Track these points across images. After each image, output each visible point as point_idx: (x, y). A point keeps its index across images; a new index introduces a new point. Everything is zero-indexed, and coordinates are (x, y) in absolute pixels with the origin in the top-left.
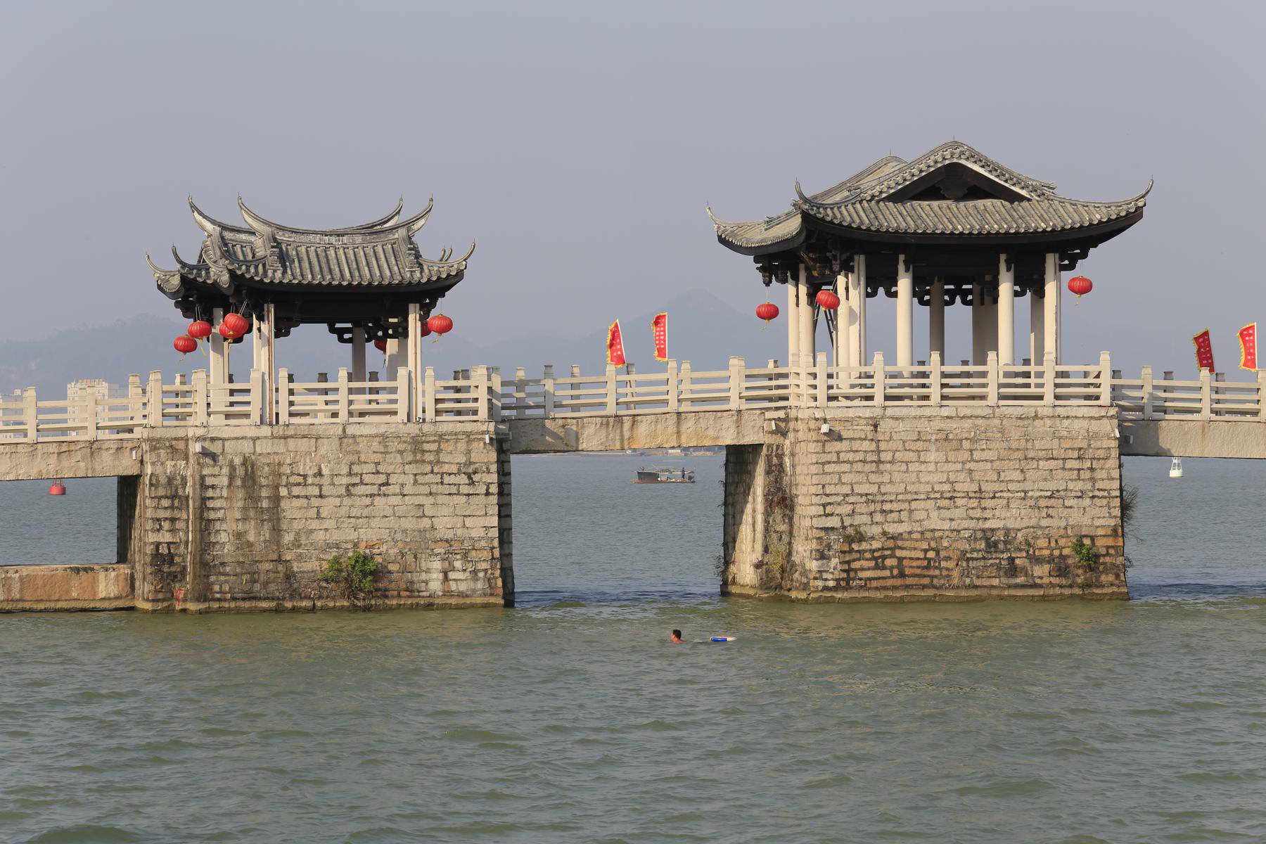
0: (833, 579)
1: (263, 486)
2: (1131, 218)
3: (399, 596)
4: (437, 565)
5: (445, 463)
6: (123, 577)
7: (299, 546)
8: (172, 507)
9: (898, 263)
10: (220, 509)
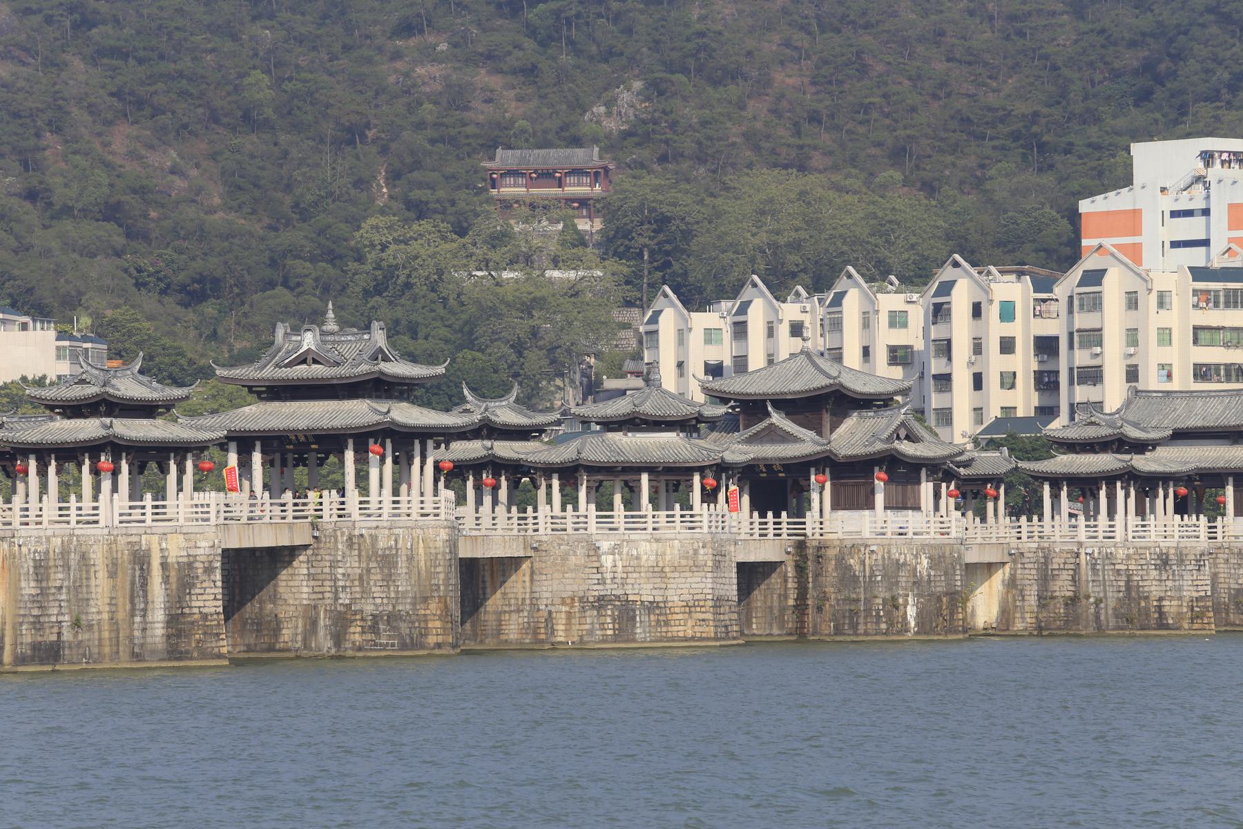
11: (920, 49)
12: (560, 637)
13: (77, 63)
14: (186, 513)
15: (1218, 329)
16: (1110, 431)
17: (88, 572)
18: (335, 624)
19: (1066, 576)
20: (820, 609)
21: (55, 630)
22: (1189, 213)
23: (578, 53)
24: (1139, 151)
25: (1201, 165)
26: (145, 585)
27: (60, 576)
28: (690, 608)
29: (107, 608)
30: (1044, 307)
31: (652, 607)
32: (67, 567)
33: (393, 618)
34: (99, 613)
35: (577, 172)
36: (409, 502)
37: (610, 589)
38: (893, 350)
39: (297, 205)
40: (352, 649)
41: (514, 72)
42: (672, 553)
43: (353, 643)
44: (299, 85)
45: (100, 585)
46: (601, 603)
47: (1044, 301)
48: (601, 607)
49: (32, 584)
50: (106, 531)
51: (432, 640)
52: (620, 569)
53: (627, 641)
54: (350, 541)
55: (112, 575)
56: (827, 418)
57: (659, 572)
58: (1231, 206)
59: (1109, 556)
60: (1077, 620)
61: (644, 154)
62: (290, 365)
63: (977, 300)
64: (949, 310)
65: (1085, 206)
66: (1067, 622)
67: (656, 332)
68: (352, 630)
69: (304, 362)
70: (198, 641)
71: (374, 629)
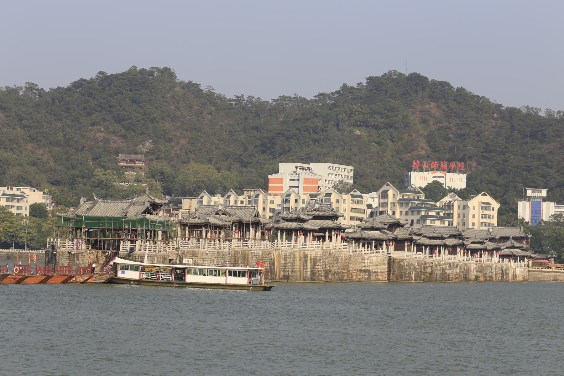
2: (405, 220)
11: (211, 137)
12: (354, 278)
13: (19, 129)
14: (309, 244)
15: (361, 209)
16: (439, 235)
17: (295, 259)
18: (325, 274)
19: (430, 268)
20: (393, 274)
21: (288, 272)
22: (294, 180)
23: (135, 133)
24: (280, 165)
25: (295, 169)
26: (306, 263)
27: (289, 259)
28: (382, 273)
29: (298, 268)
30: (312, 201)
31: (375, 272)
32: (291, 257)
33: (338, 273)
34: (297, 269)
35: (139, 160)
36: (277, 243)
37: (367, 268)
38: (270, 209)
39: (71, 165)
40: (329, 280)
41: (120, 136)
42: (379, 260)
43: (330, 278)
44: (70, 136)
45: (297, 262)
46: (365, 271)
47: (312, 200)
48: (365, 272)
49: (283, 261)
50: (299, 249)
51: (345, 278)
52: (369, 263)
53: (370, 280)
54: (330, 254)
55: (300, 260)
56: (394, 229)
57: (376, 264)
58: (304, 179)
59: (439, 264)
60: (432, 278)
61: (153, 157)
62: (311, 211)
63: (296, 199)
64: (290, 200)
65: (270, 176)
66: (429, 279)
67: (202, 201)
68: (329, 275)
69: (315, 211)
70: (317, 277)
71: (334, 275)
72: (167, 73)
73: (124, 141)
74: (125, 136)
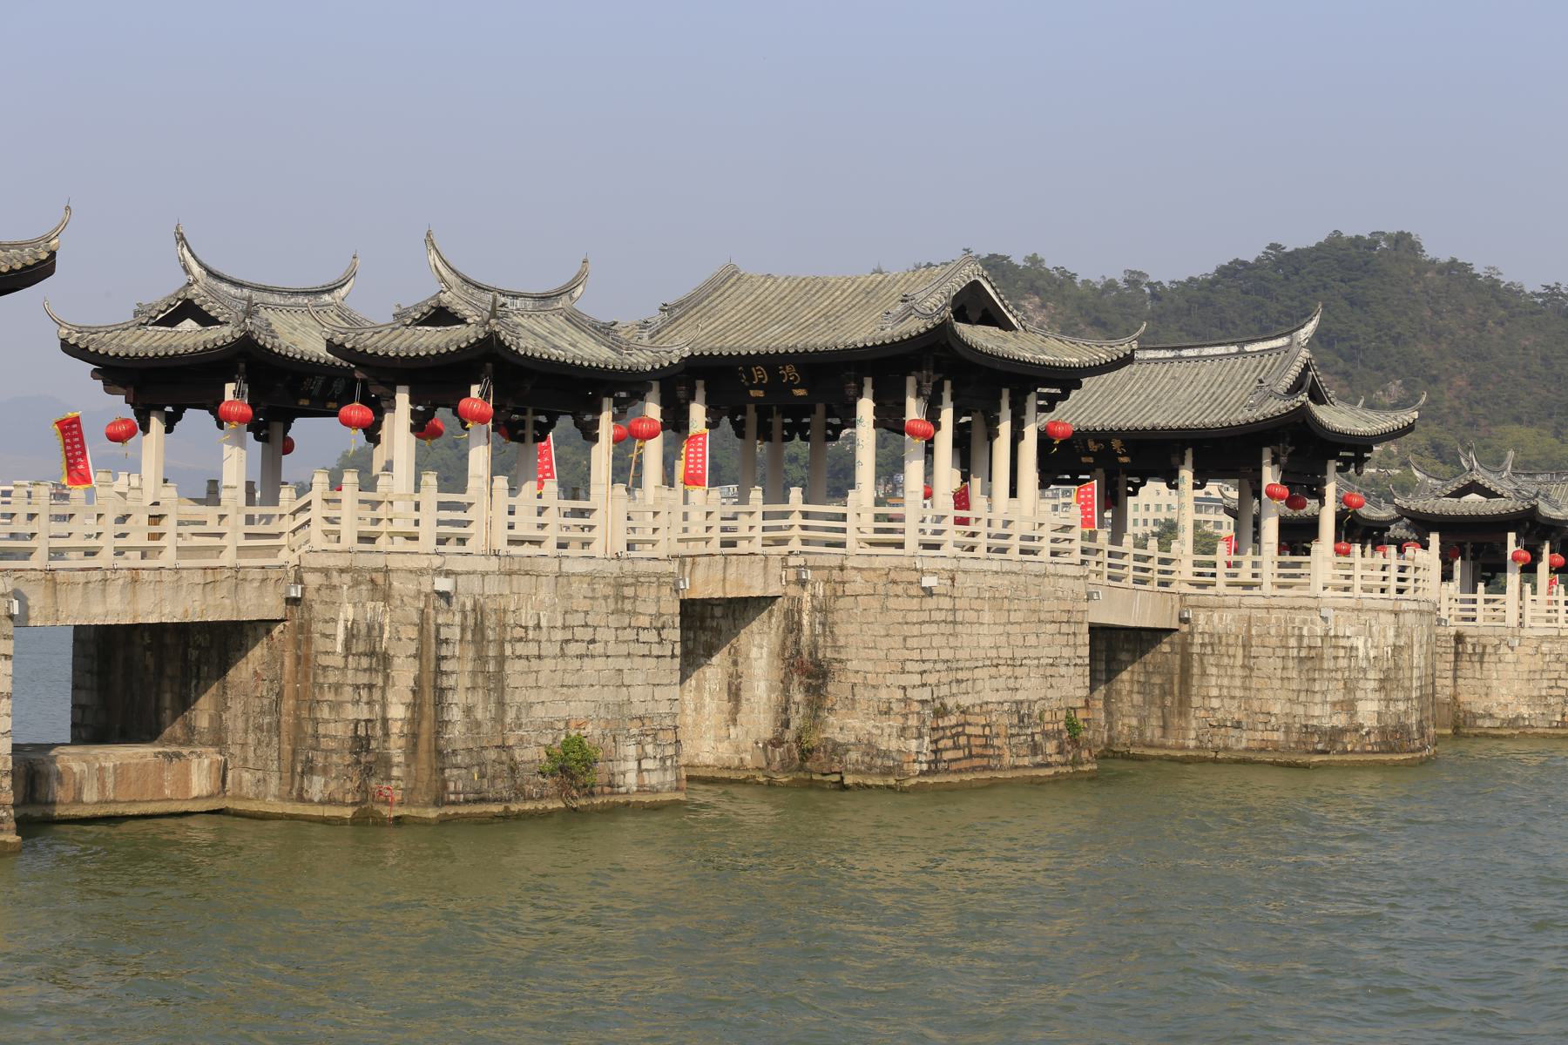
0: (926, 762)
1: (491, 642)
3: (603, 793)
4: (632, 750)
5: (640, 613)
6: (216, 765)
7: (520, 726)
8: (370, 670)
9: (1001, 397)
10: (453, 673)
41: (1336, 373)
72: (1404, 244)
73: (1345, 383)
74: (1344, 373)
